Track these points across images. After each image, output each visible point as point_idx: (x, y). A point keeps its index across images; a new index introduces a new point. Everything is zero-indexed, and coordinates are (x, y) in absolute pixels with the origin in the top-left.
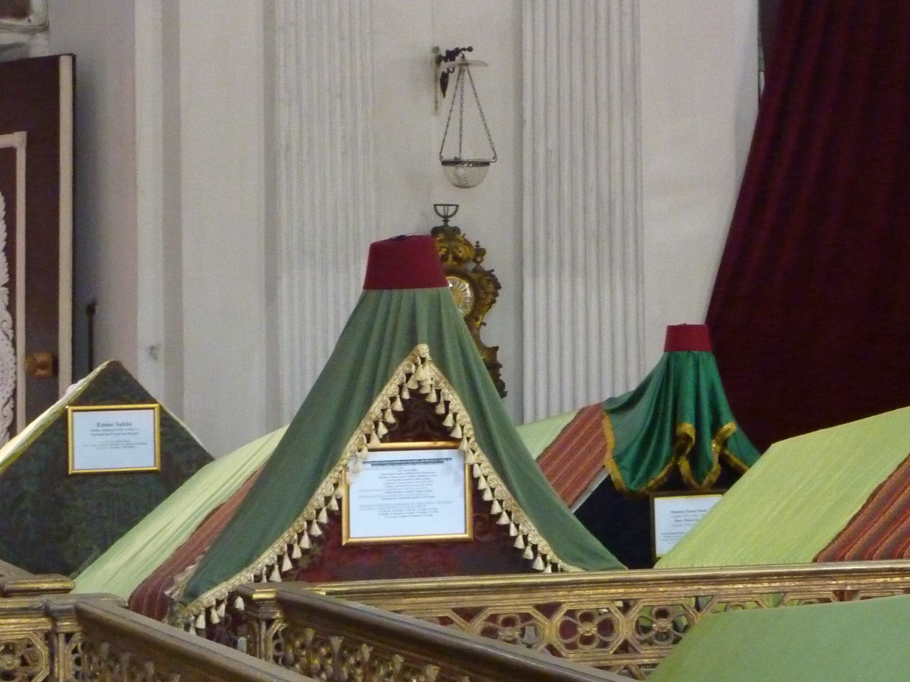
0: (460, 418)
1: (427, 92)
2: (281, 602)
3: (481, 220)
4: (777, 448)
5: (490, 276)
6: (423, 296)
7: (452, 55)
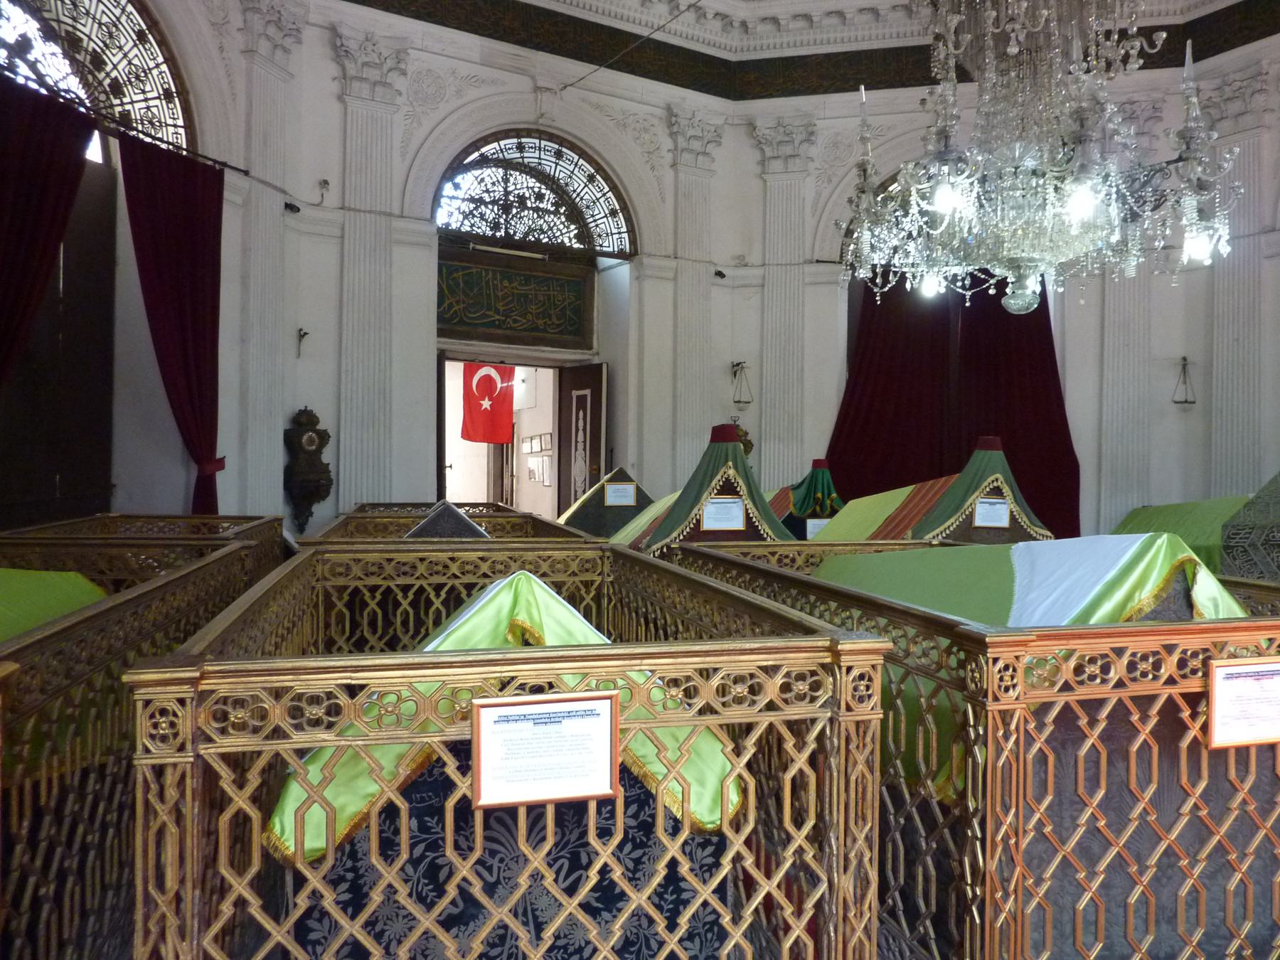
0: (742, 488)
1: (729, 378)
2: (681, 549)
3: (747, 422)
4: (851, 502)
5: (750, 442)
6: (730, 445)
7: (738, 365)
